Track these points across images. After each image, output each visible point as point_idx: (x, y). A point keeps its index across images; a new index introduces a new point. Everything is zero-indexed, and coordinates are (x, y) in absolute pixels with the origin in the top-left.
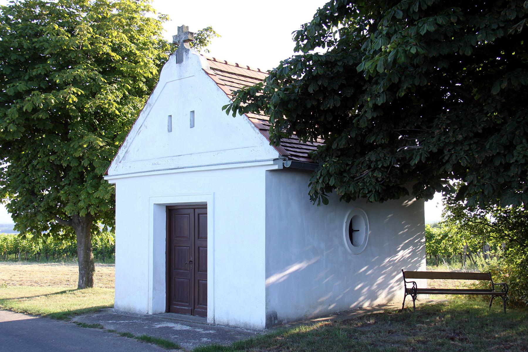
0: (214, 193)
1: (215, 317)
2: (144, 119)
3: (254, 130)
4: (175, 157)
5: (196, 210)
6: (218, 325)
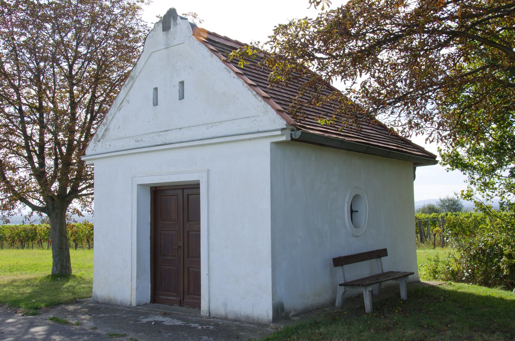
0: (208, 170)
1: (211, 310)
2: (126, 93)
3: (256, 98)
4: (162, 133)
5: (185, 191)
6: (214, 318)
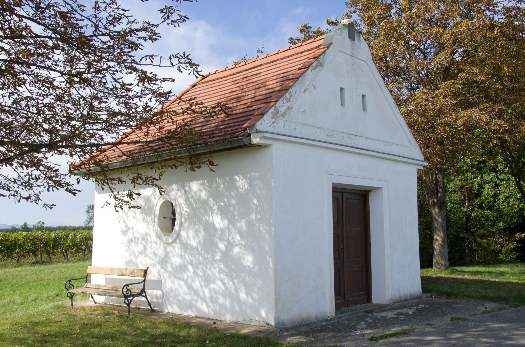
4: (352, 136)
